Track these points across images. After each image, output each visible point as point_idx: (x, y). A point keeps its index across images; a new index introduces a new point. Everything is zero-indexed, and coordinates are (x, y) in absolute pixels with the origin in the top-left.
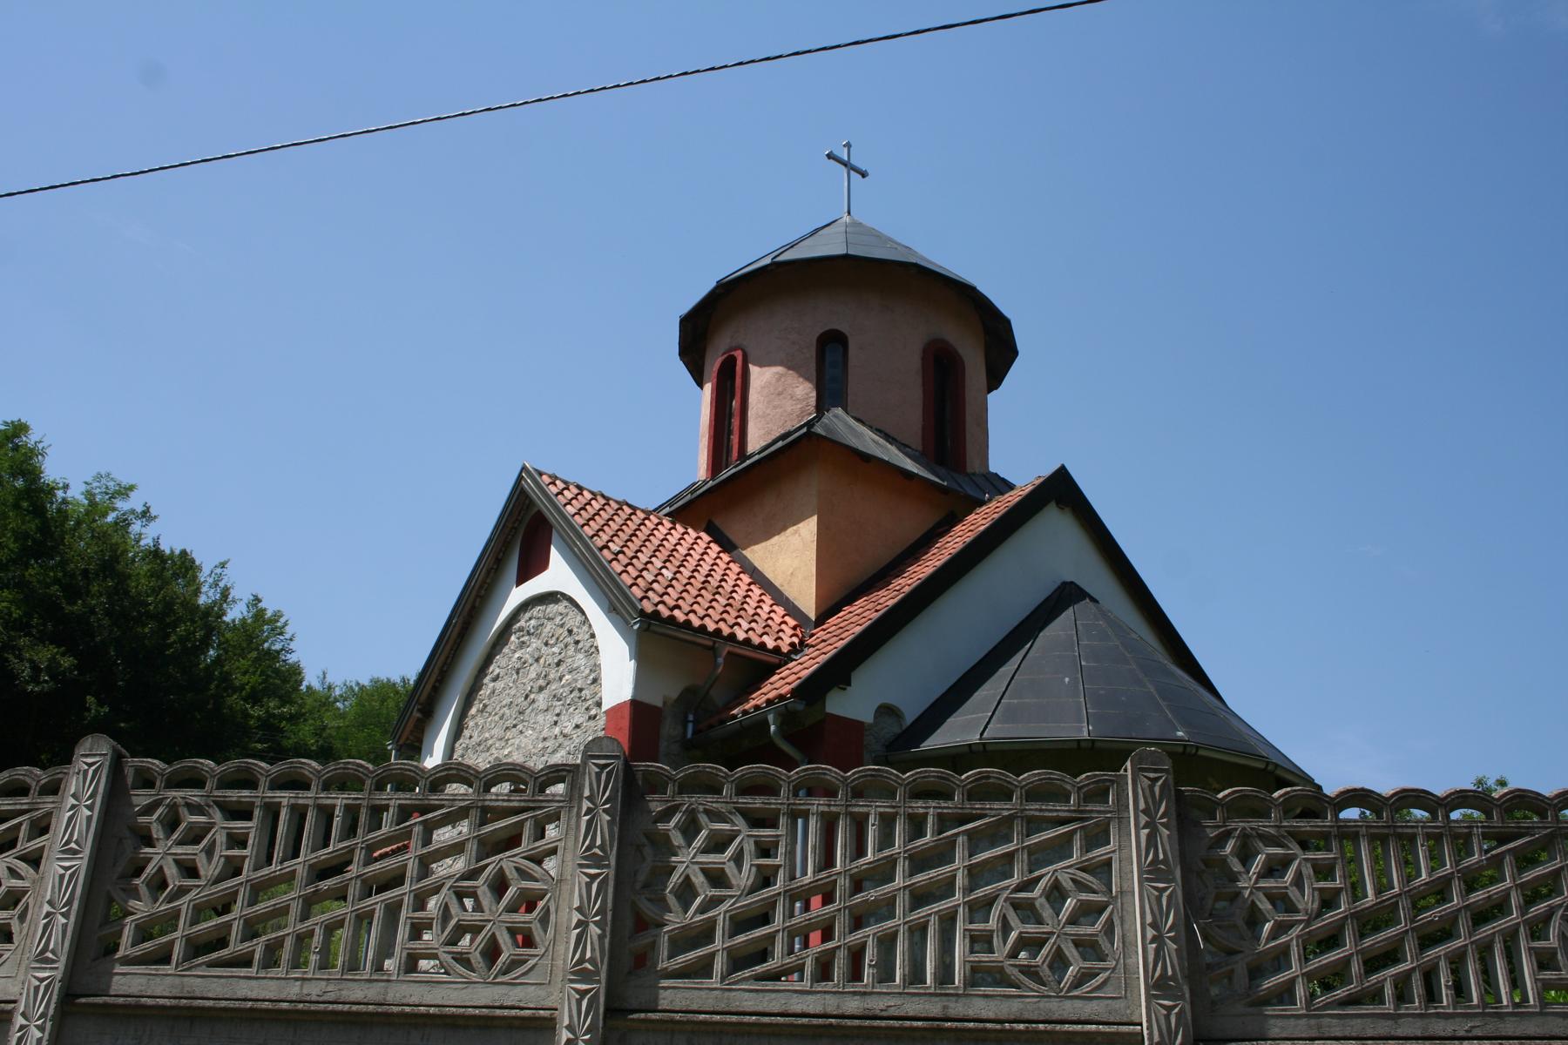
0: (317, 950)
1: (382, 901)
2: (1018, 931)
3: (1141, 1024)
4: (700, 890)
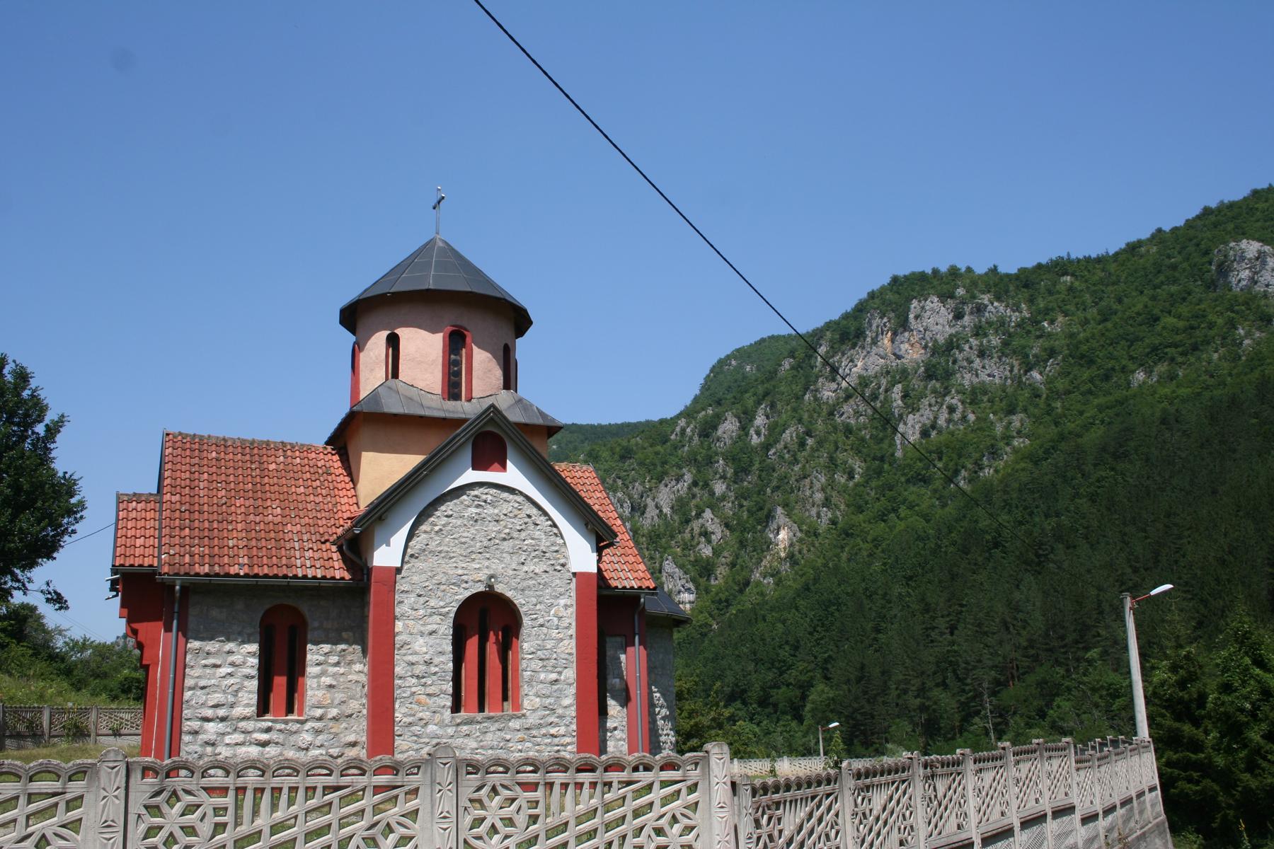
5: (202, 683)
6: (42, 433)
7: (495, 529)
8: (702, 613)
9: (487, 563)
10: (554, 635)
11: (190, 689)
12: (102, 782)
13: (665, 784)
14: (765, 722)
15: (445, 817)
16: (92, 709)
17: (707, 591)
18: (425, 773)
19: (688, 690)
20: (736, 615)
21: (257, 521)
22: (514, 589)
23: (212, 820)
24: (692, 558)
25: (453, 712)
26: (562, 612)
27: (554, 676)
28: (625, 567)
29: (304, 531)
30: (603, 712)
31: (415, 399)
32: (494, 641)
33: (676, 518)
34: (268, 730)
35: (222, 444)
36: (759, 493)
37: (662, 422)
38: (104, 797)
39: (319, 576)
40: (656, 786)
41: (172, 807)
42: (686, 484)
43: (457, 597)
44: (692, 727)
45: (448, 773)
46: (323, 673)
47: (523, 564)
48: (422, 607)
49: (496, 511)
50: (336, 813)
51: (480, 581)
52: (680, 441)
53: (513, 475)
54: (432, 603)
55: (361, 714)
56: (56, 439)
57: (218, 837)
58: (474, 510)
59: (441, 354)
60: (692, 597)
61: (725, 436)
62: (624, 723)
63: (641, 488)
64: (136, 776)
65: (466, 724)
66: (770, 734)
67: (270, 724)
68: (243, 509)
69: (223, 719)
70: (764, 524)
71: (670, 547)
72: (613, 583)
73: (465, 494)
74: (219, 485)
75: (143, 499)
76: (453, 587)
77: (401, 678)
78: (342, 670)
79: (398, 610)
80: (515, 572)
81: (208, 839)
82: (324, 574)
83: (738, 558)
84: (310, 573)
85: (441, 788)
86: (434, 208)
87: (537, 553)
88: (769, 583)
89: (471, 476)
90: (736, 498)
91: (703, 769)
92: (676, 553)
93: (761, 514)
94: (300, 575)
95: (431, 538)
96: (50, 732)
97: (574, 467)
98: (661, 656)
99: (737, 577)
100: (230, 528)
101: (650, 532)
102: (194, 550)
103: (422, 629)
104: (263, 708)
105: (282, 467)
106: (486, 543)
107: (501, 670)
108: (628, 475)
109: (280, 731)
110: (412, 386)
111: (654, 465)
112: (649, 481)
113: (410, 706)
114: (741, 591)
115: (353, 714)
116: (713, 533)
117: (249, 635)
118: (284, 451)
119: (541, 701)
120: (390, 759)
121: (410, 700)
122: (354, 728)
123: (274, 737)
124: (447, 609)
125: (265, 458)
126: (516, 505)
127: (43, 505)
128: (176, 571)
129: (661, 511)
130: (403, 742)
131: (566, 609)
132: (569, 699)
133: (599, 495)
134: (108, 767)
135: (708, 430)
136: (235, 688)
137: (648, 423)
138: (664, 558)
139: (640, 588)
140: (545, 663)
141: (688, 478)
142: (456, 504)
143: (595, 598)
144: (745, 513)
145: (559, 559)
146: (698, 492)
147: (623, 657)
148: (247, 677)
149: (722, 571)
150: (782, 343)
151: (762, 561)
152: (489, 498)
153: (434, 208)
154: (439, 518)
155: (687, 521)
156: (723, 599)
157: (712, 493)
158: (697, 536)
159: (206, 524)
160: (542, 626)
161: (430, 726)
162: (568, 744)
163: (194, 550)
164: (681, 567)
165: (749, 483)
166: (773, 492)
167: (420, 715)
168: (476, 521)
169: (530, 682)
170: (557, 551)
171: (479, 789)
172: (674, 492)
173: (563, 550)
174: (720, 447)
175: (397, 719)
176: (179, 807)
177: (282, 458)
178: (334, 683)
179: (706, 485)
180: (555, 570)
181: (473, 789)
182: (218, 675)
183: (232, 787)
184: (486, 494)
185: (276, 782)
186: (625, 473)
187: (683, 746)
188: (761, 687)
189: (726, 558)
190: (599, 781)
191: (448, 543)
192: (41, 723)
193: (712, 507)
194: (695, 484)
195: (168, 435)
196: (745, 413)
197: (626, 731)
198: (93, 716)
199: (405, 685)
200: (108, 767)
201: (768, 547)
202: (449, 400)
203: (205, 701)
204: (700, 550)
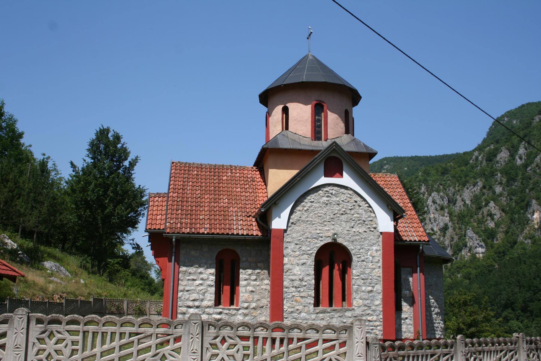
5: (187, 288)
6: (128, 166)
7: (337, 209)
8: (489, 259)
9: (333, 227)
10: (370, 266)
11: (181, 291)
12: (15, 325)
13: (325, 341)
14: (526, 321)
15: (194, 353)
16: (147, 301)
17: (492, 247)
18: (185, 327)
19: (470, 300)
20: (508, 260)
21: (215, 206)
22: (348, 241)
23: (70, 347)
24: (483, 229)
25: (314, 306)
26: (375, 254)
27: (370, 288)
28: (412, 229)
29: (239, 211)
30: (399, 309)
31: (297, 140)
32: (338, 269)
33: (474, 206)
34: (220, 313)
35: (200, 167)
36: (521, 192)
37: (465, 153)
38: (16, 333)
39: (245, 234)
40: (320, 342)
41: (51, 340)
42: (479, 188)
43: (316, 245)
44: (471, 321)
45: (197, 328)
46: (248, 285)
47: (353, 227)
48: (298, 250)
49: (338, 199)
50: (136, 348)
51: (329, 236)
52: (475, 164)
53: (346, 180)
54: (303, 248)
55: (268, 307)
56: (134, 168)
57: (74, 357)
58: (326, 199)
60: (483, 250)
61: (501, 160)
62: (412, 316)
63: (453, 190)
64: (33, 323)
65: (322, 313)
66: (529, 328)
67: (221, 310)
68: (208, 200)
69: (198, 307)
70: (525, 210)
71: (471, 222)
72: (404, 238)
73: (321, 190)
74: (197, 188)
75: (162, 195)
77: (287, 288)
78: (258, 283)
79: (285, 252)
80: (348, 232)
81: (68, 357)
82: (247, 233)
83: (510, 229)
84: (240, 232)
85: (192, 336)
86: (308, 38)
87: (360, 221)
88: (528, 243)
89: (324, 180)
90: (508, 195)
91: (349, 334)
92: (474, 226)
93: (523, 204)
94: (235, 233)
95: (303, 214)
96: (127, 312)
97: (386, 175)
98: (435, 279)
99: (509, 239)
100: (201, 209)
101: (459, 214)
102: (183, 221)
103: (298, 262)
104: (218, 302)
105: (229, 178)
106: (332, 216)
107: (341, 285)
108: (446, 183)
109: (226, 314)
110: (296, 134)
111: (461, 177)
112: (458, 186)
113: (291, 302)
114: (512, 247)
115: (264, 306)
116: (495, 215)
117: (210, 264)
118: (231, 170)
119: (363, 302)
120: (166, 319)
121: (292, 300)
122: (264, 314)
123: (223, 317)
124: (311, 252)
125: (221, 174)
126: (349, 196)
127: (128, 201)
128: (173, 232)
129: (465, 203)
130: (288, 322)
131: (377, 252)
132: (378, 301)
133: (399, 190)
134: (18, 318)
135: (491, 157)
136: (203, 291)
137: (458, 155)
138: (467, 228)
139: (420, 241)
140: (365, 281)
141: (480, 184)
142: (316, 195)
143: (393, 246)
144: (514, 203)
145: (372, 224)
146: (486, 192)
147: (411, 279)
148: (210, 286)
149: (500, 236)
150: (535, 107)
151: (524, 230)
152: (334, 192)
153: (308, 38)
154: (307, 203)
155: (480, 208)
156: (501, 251)
157: (494, 192)
158: (486, 216)
159: (190, 208)
160: (363, 261)
161: (302, 314)
162: (378, 326)
163: (183, 221)
164: (477, 233)
165: (516, 186)
166: (530, 191)
167: (297, 307)
168: (327, 204)
169: (357, 291)
170: (371, 221)
171: (216, 338)
172: (472, 192)
173: (375, 220)
174: (498, 167)
175: (285, 309)
176: (54, 340)
177: (230, 174)
178: (254, 290)
179: (491, 188)
180: (370, 231)
181: (212, 338)
182: (195, 284)
183: (81, 331)
184: (332, 190)
185: (104, 329)
186: (444, 182)
187: (466, 332)
188: (523, 301)
189: (503, 228)
190: (286, 337)
192: (123, 307)
193: (494, 200)
194: (484, 187)
195: (173, 163)
196: (513, 147)
197: (412, 320)
198: (148, 305)
199: (289, 291)
200: (18, 318)
201: (528, 222)
202: (315, 140)
203: (189, 298)
204: (488, 224)
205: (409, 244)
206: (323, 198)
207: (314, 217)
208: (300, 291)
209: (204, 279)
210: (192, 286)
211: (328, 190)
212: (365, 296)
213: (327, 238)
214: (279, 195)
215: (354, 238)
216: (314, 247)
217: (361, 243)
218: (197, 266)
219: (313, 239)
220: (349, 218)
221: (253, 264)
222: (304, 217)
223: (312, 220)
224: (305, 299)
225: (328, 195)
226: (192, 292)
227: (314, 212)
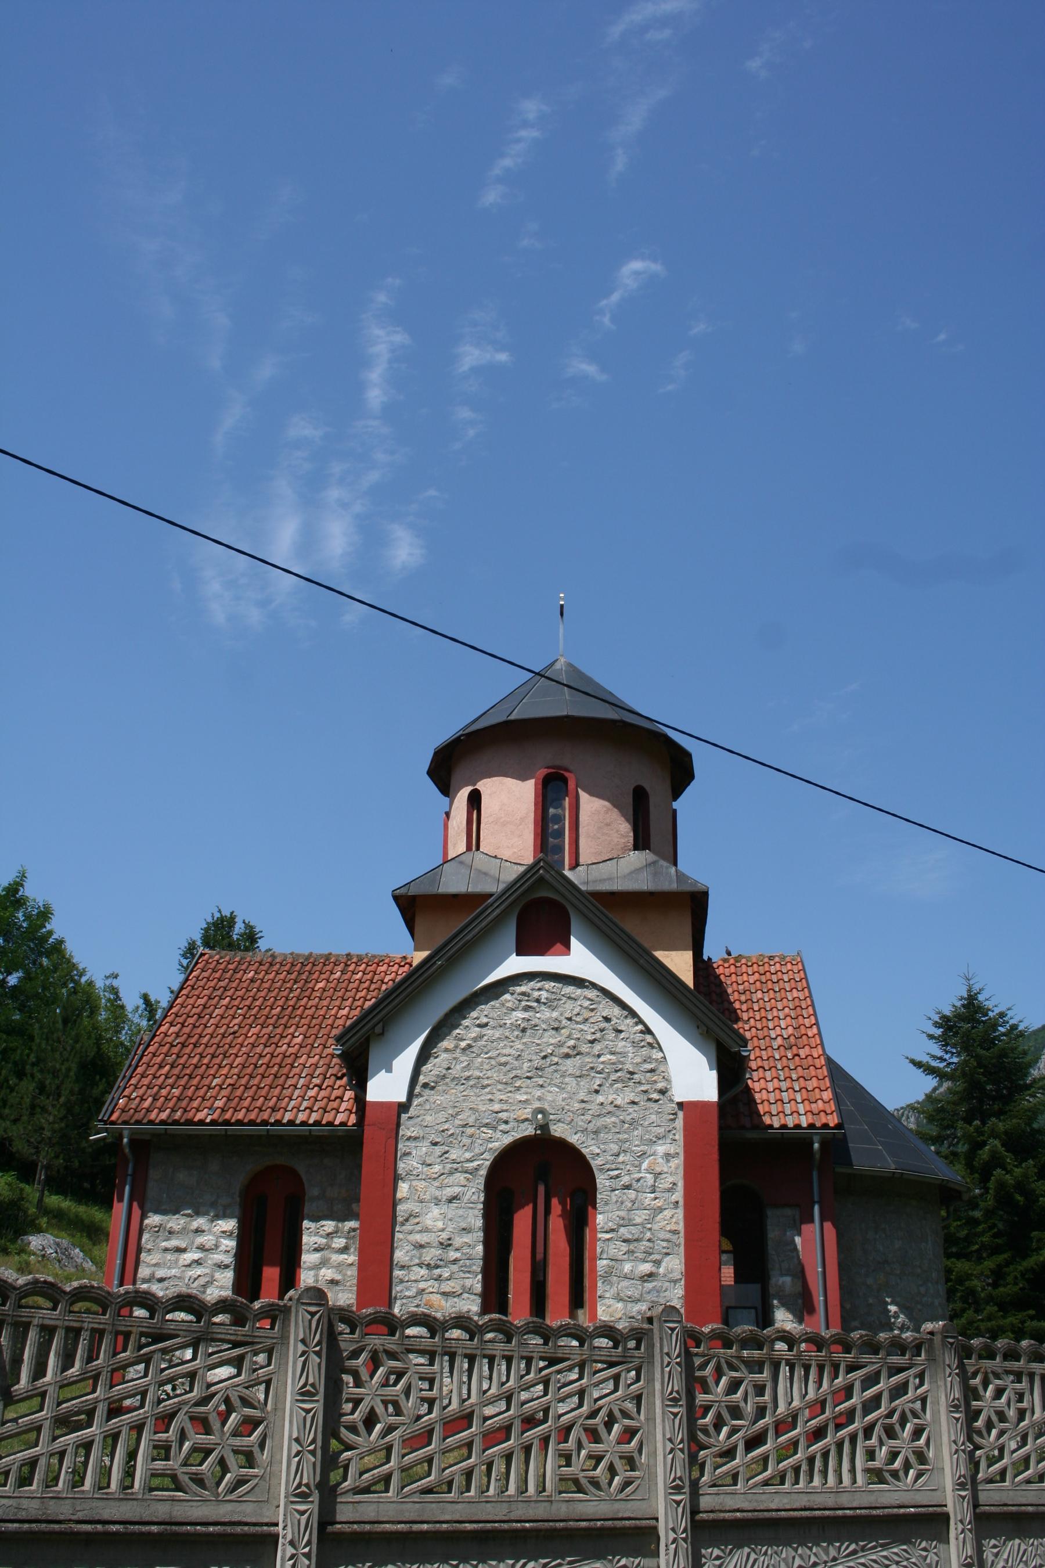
0: (70, 1470)
1: (127, 1424)
2: (192, 1443)
3: (657, 1519)
4: (381, 1419)
5: (160, 1273)
7: (552, 1041)
9: (538, 1093)
26: (661, 1166)
27: (646, 1268)
32: (559, 1212)
43: (490, 1146)
46: (324, 1263)
47: (597, 1092)
48: (439, 1160)
49: (555, 1014)
51: (527, 1120)
54: (454, 1155)
58: (520, 1015)
59: (533, 808)
76: (484, 1129)
77: (403, 1267)
79: (402, 1166)
80: (584, 1105)
87: (619, 1074)
89: (515, 964)
95: (455, 1058)
103: (438, 1193)
106: (537, 1062)
110: (495, 857)
117: (225, 1207)
121: (417, 1302)
124: (476, 1163)
126: (587, 1003)
131: (668, 1161)
139: (811, 1126)
140: (632, 1247)
142: (493, 1008)
145: (655, 1082)
147: (798, 1240)
148: (219, 1266)
152: (544, 995)
154: (467, 1030)
160: (627, 1187)
168: (524, 1030)
170: (652, 1071)
178: (338, 1277)
180: (649, 1100)
182: (181, 1262)
184: (540, 989)
191: (480, 1066)
205: (780, 1136)
206: (514, 1013)
207: (486, 1067)
208: (440, 1276)
209: (207, 1247)
210: (174, 1268)
211: (528, 991)
212: (631, 1289)
213: (521, 1125)
214: (387, 1005)
215: (600, 1122)
216: (482, 1151)
217: (620, 1136)
218: (189, 1211)
219: (482, 1129)
220: (586, 1066)
221: (340, 1206)
222: (458, 1067)
223: (481, 1075)
224: (455, 1299)
225: (528, 1003)
226: (172, 1283)
227: (486, 1053)
